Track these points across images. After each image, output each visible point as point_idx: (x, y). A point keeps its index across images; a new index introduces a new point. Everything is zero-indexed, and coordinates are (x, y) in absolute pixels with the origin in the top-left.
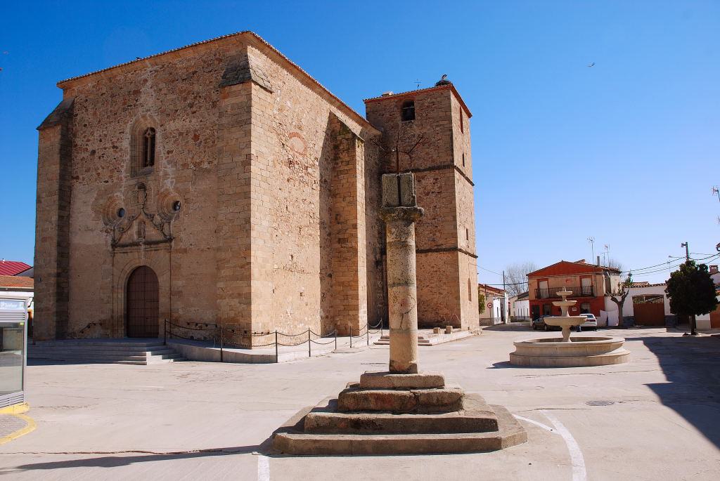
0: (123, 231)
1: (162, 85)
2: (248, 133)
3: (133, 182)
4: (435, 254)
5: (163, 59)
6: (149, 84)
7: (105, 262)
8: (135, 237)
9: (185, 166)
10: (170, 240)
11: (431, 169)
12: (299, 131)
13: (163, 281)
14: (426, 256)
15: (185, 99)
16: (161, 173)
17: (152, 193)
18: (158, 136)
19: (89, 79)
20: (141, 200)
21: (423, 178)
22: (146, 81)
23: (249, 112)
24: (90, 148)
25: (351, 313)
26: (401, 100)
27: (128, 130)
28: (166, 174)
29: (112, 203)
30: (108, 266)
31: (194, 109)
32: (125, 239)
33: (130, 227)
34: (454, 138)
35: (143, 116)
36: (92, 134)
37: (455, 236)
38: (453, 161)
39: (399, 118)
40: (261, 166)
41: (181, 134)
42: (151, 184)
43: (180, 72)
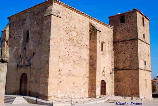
0: (20, 62)
1: (31, 17)
2: (50, 31)
3: (23, 47)
4: (131, 70)
5: (32, 9)
6: (28, 17)
7: (15, 72)
8: (23, 64)
9: (36, 42)
10: (31, 65)
11: (130, 40)
12: (75, 29)
13: (28, 77)
14: (128, 71)
15: (37, 21)
16: (30, 44)
17: (27, 50)
18: (30, 32)
19: (14, 16)
20: (25, 53)
21: (127, 43)
22: (27, 16)
23: (50, 24)
24: (14, 37)
25: (94, 90)
26: (120, 16)
27: (23, 31)
28: (31, 44)
29: (18, 53)
30: (16, 73)
31: (39, 24)
32: (20, 64)
33: (21, 61)
34: (138, 28)
35: (26, 27)
36: (14, 32)
37: (137, 64)
38: (137, 37)
39: (120, 22)
40: (55, 42)
41: (35, 32)
42: (27, 48)
43: (36, 12)
